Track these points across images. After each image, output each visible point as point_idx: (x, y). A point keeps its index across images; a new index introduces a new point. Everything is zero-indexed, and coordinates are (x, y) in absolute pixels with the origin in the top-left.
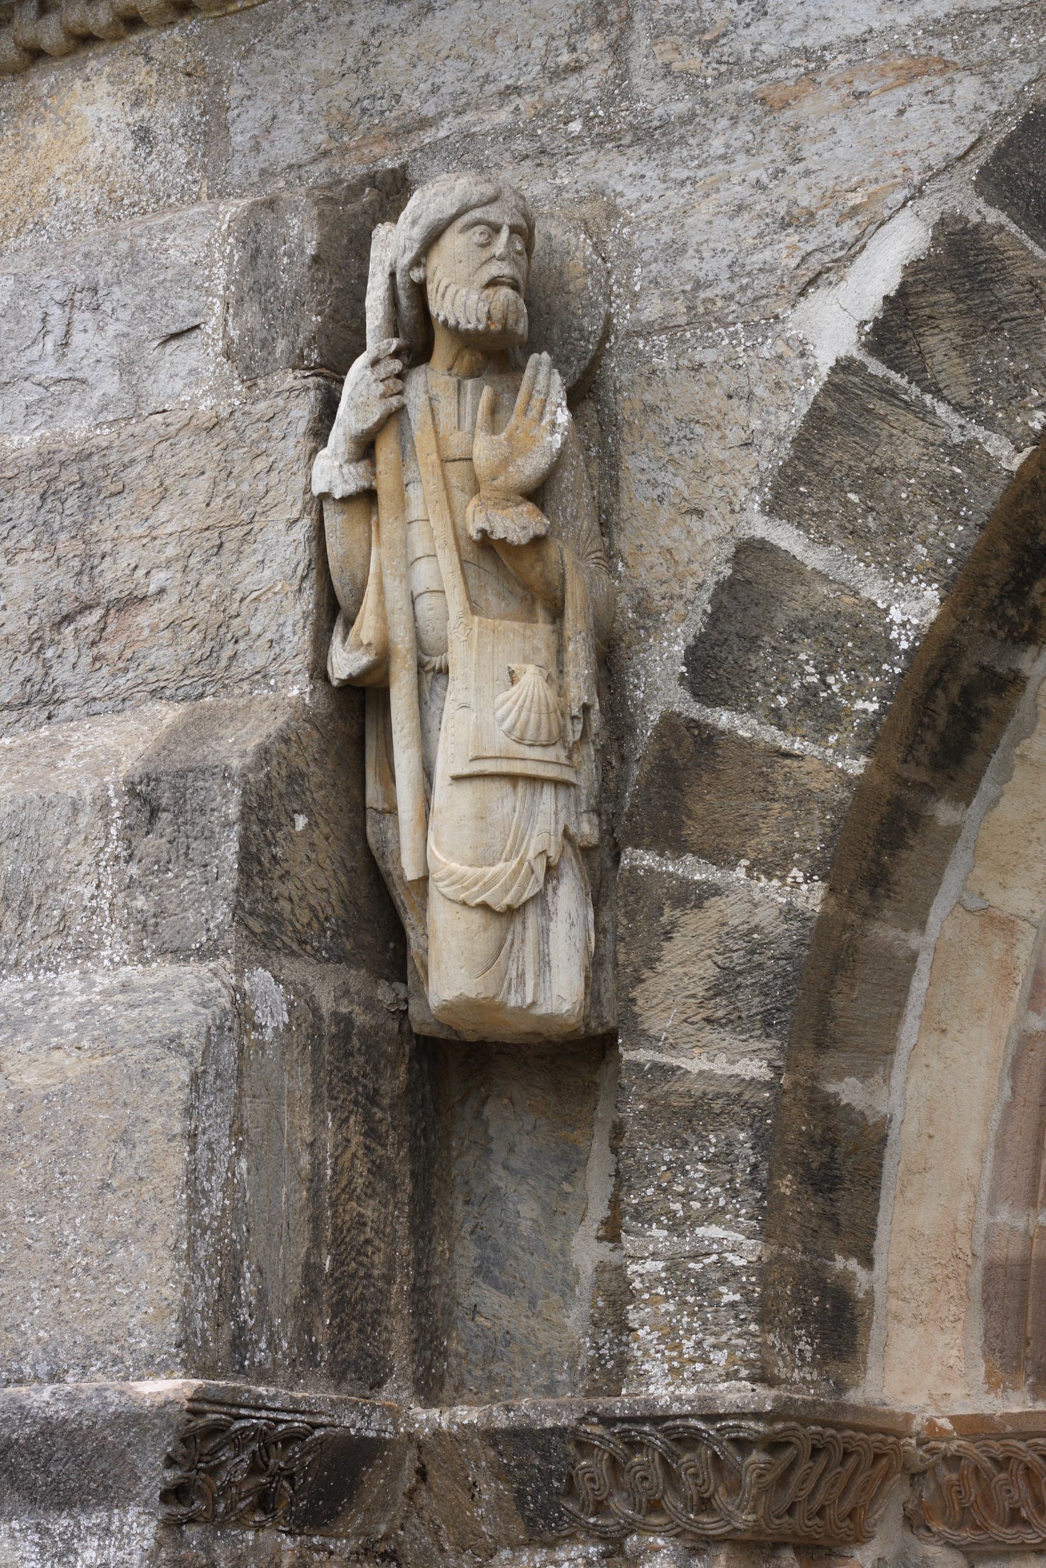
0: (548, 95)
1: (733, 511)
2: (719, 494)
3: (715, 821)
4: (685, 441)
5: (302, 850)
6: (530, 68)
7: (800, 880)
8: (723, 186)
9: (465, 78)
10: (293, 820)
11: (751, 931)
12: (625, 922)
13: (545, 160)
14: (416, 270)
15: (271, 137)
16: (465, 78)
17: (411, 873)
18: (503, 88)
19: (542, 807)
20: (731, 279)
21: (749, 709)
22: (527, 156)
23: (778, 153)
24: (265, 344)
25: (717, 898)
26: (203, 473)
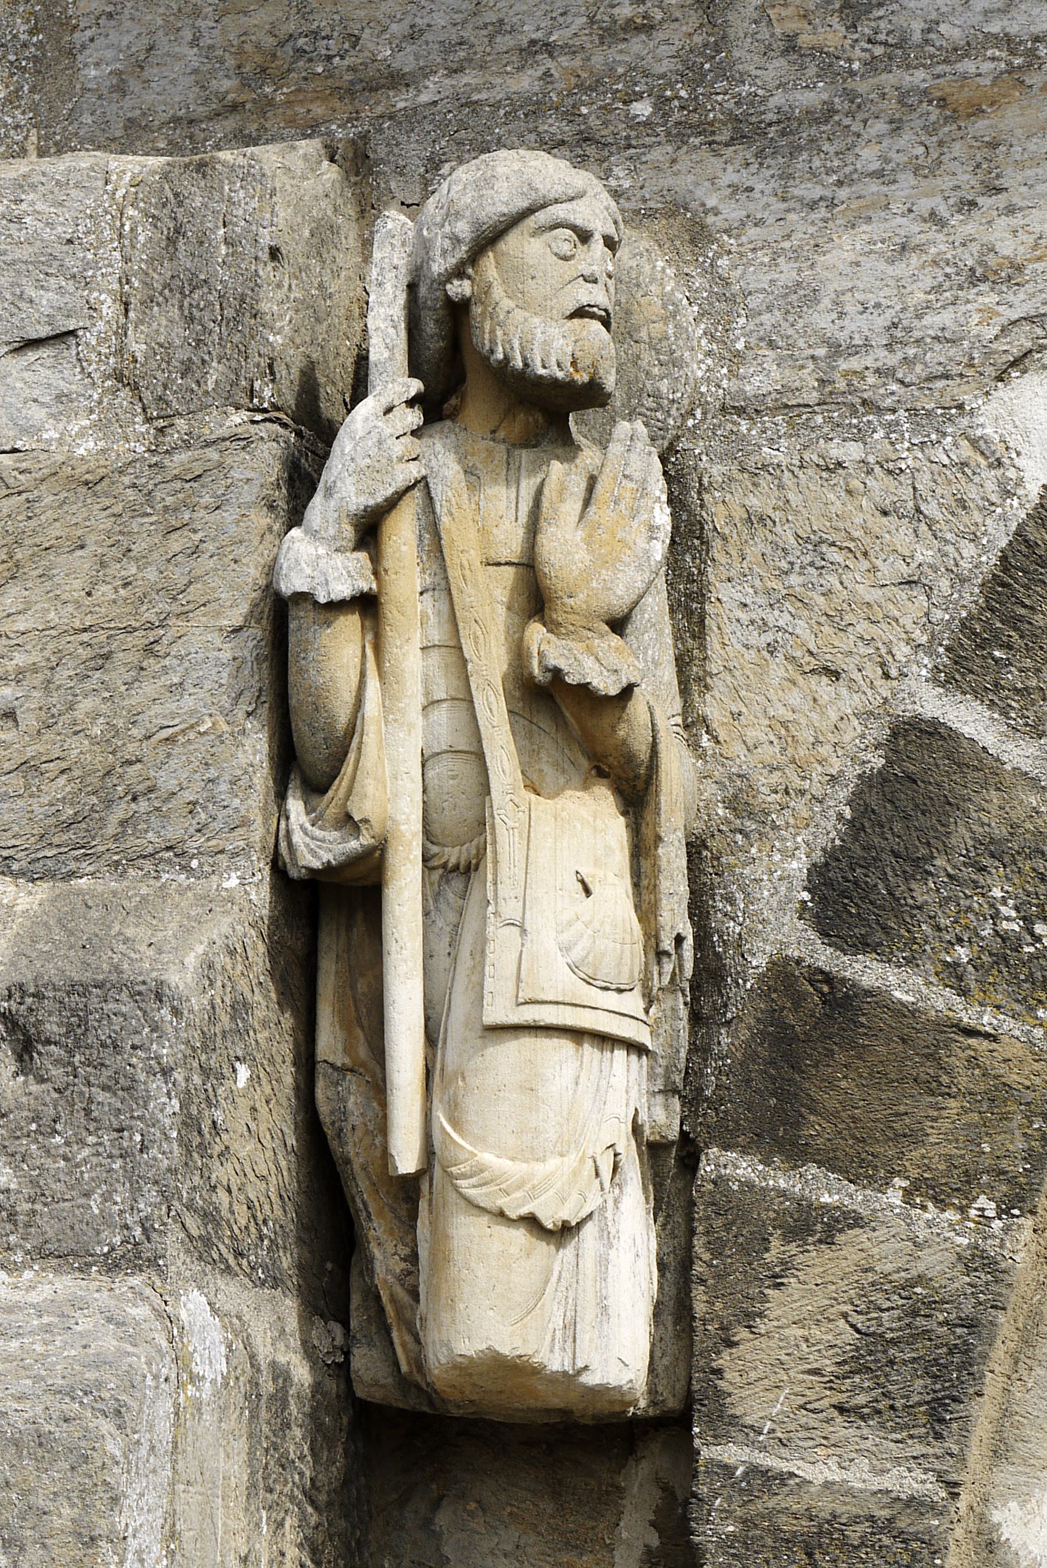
0: (598, 60)
1: (887, 676)
2: (864, 650)
3: (854, 1119)
4: (811, 570)
6: (569, 19)
7: (991, 1213)
8: (878, 214)
9: (465, 22)
11: (911, 1283)
12: (706, 1256)
13: (591, 150)
14: (456, 282)
15: (145, 74)
16: (465, 22)
17: (406, 1159)
18: (525, 43)
20: (889, 347)
21: (910, 961)
22: (563, 143)
23: (966, 178)
25: (857, 1231)
26: (82, 547)
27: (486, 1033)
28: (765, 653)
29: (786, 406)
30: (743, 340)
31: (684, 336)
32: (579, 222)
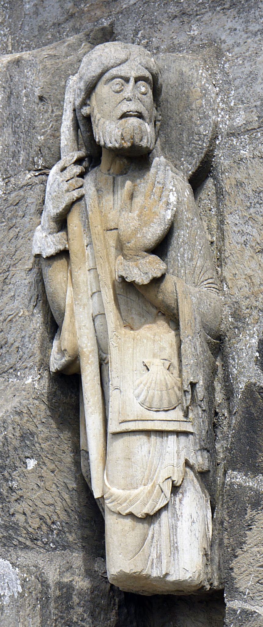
5: (33, 481)
10: (25, 463)
12: (227, 519)
13: (185, 19)
14: (84, 108)
19: (168, 449)
22: (176, 16)
24: (15, 155)
27: (113, 436)
28: (243, 245)
29: (248, 130)
30: (233, 101)
31: (209, 104)
32: (123, 74)
